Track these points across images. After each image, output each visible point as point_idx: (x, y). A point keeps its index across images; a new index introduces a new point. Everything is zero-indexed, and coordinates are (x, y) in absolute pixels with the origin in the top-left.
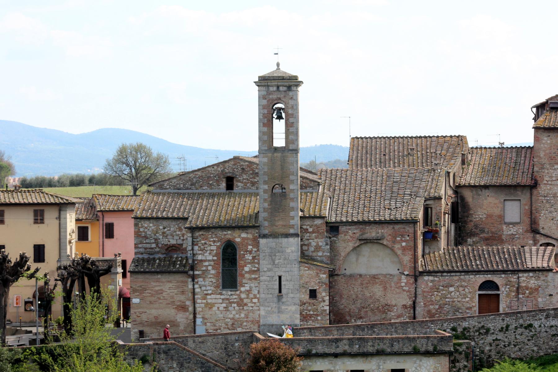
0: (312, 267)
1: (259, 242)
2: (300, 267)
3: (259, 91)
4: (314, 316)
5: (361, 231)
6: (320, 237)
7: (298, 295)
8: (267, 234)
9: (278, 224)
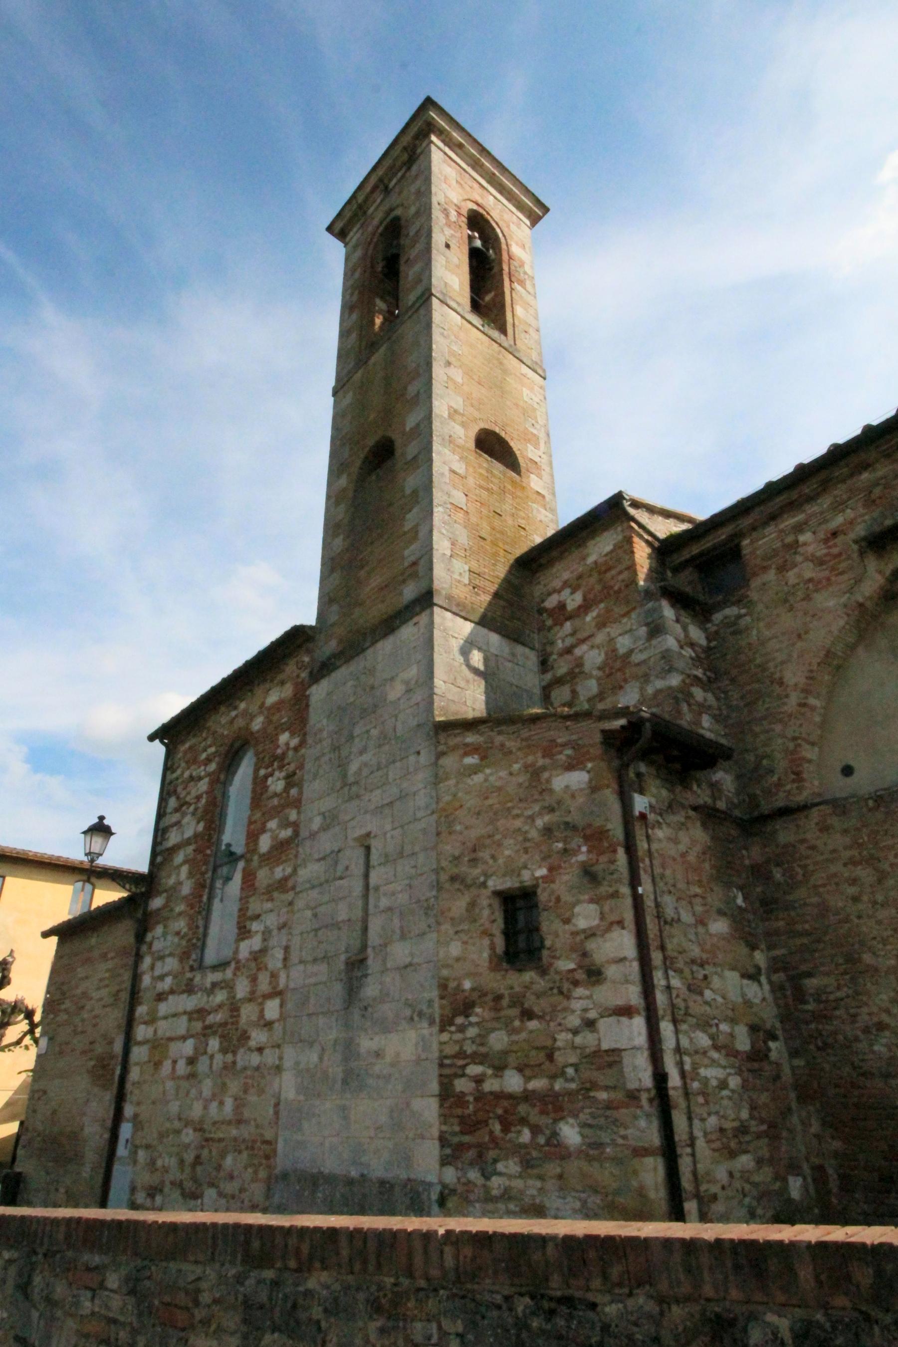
0: (499, 739)
2: (440, 755)
4: (535, 1117)
6: (618, 610)
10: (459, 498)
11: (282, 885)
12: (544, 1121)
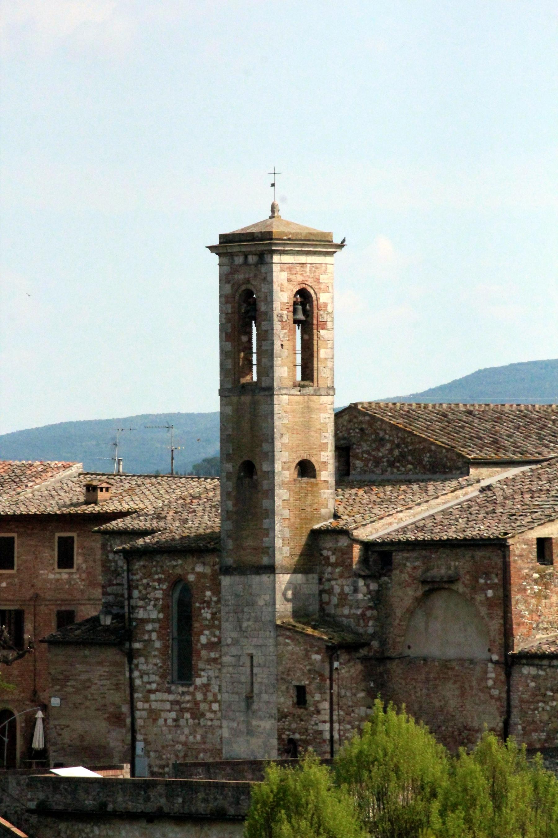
1: (220, 584)
2: (278, 636)
3: (220, 265)
5: (424, 563)
7: (274, 698)
8: (230, 567)
9: (247, 544)
10: (286, 513)
11: (215, 660)
12: (305, 746)
